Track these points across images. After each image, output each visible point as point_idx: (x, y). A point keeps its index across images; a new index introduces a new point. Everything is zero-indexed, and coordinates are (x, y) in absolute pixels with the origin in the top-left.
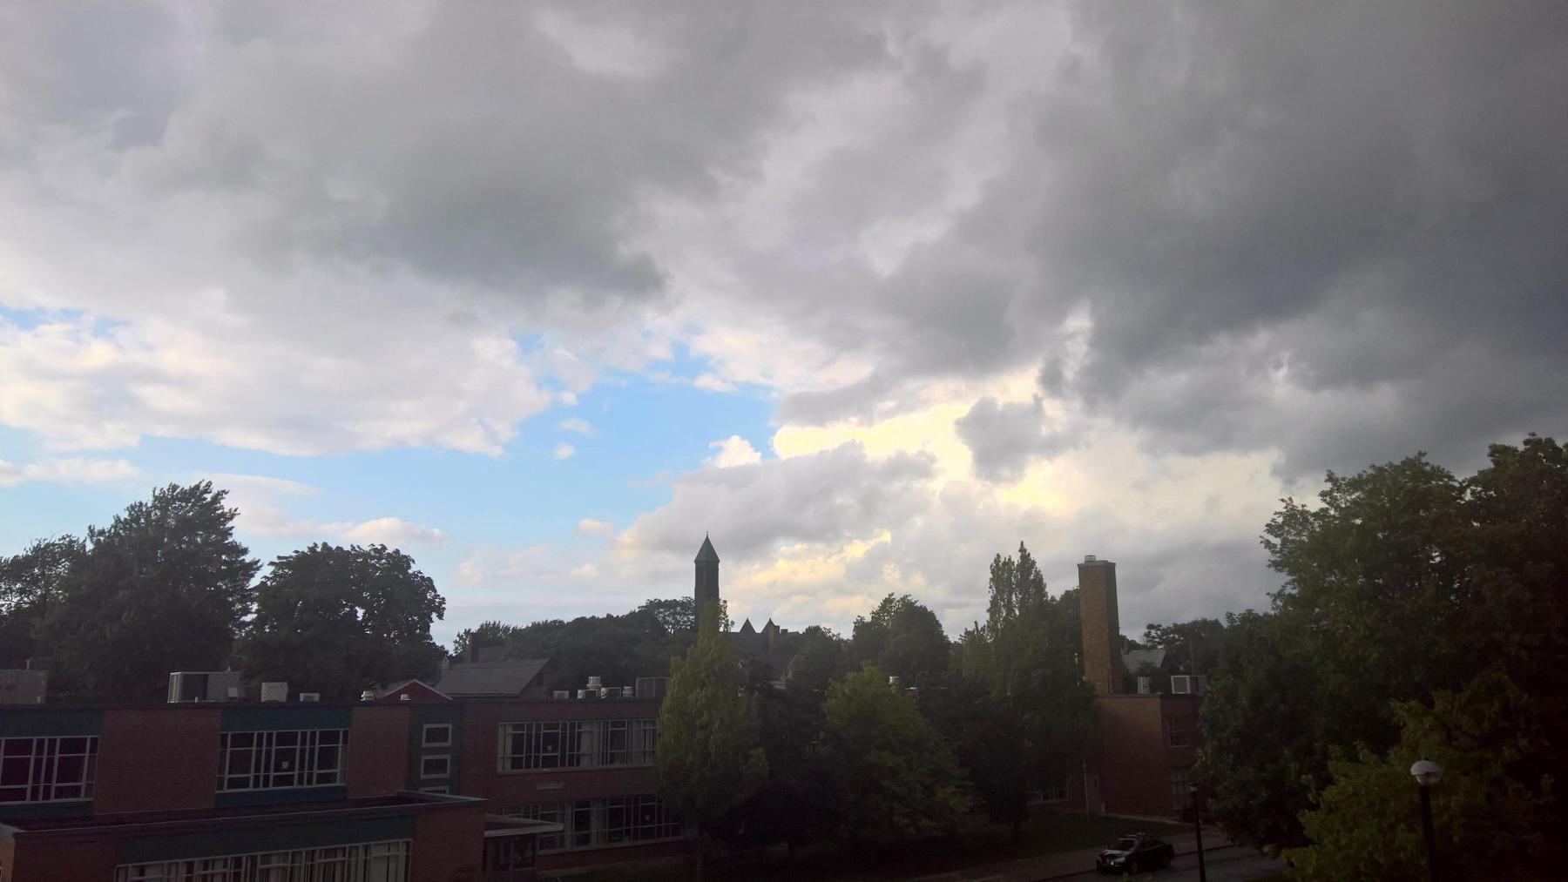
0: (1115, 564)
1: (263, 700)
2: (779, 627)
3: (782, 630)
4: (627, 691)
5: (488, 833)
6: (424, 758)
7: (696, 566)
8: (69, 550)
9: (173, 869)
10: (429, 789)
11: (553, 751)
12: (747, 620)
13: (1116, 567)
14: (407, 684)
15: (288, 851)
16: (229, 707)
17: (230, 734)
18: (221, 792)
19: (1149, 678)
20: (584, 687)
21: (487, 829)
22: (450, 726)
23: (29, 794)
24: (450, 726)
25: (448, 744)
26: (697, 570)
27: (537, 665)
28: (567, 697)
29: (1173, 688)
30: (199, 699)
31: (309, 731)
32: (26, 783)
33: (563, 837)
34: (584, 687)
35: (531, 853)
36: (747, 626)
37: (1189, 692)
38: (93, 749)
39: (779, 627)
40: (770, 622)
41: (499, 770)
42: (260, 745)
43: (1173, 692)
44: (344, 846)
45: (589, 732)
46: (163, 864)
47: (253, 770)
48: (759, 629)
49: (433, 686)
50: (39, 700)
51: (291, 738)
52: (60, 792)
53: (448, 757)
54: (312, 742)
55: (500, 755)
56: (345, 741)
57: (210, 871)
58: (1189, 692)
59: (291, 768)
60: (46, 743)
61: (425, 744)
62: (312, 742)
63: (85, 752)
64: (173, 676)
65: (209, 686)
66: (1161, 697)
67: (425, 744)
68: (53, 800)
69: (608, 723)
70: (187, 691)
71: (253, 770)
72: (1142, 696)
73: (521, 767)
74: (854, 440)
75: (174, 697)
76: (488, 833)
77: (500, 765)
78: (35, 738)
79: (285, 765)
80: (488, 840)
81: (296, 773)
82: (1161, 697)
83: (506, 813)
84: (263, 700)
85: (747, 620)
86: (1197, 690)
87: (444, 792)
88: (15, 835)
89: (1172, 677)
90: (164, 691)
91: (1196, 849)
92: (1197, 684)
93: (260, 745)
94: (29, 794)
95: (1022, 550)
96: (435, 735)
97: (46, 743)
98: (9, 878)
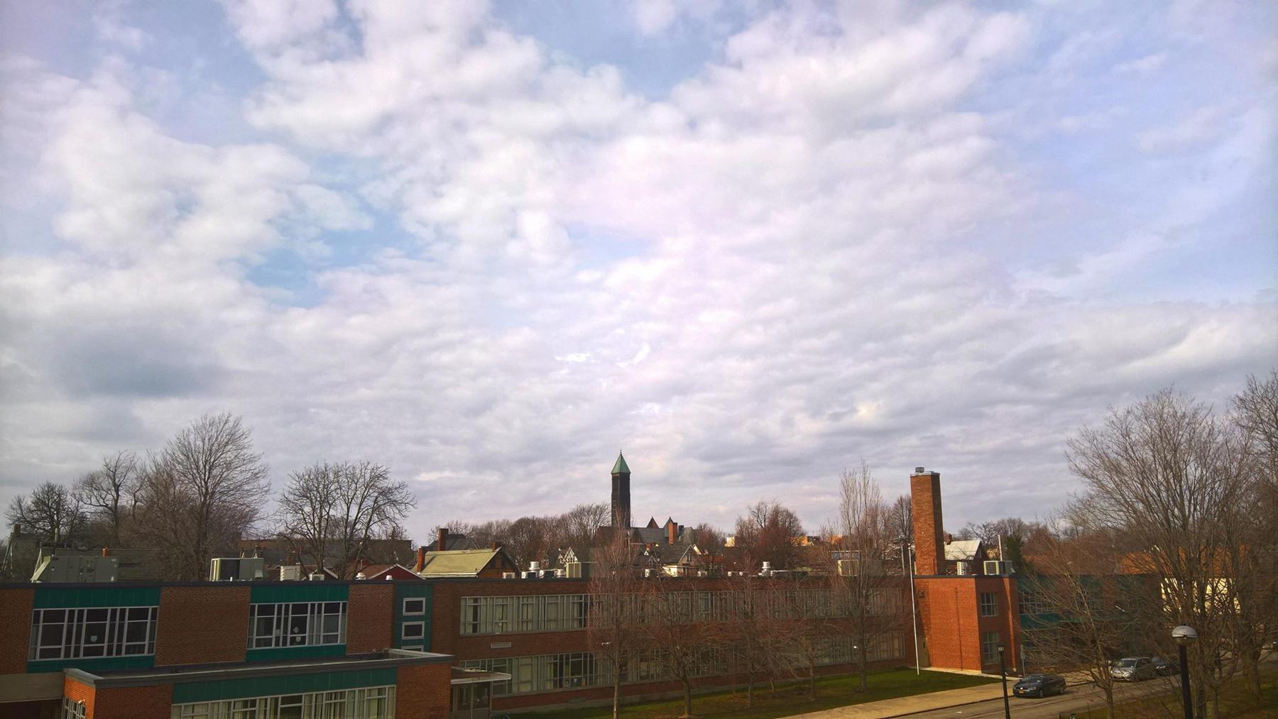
0: (939, 474)
1: (282, 579)
2: (677, 524)
5: (454, 681)
9: (216, 707)
10: (408, 647)
11: (97, 642)
12: (652, 519)
15: (208, 702)
16: (256, 584)
17: (257, 605)
18: (111, 657)
20: (527, 570)
21: (453, 679)
22: (423, 599)
23: (105, 651)
24: (423, 599)
25: (423, 613)
26: (613, 479)
30: (233, 579)
31: (284, 604)
32: (60, 644)
33: (511, 684)
34: (527, 570)
35: (487, 697)
37: (998, 573)
38: (154, 617)
39: (677, 524)
41: (462, 632)
42: (279, 613)
43: (986, 574)
44: (266, 697)
46: (208, 704)
47: (147, 638)
48: (661, 524)
50: (112, 579)
51: (102, 615)
52: (128, 650)
54: (287, 613)
55: (462, 620)
56: (344, 611)
57: (333, 701)
59: (101, 640)
61: (405, 613)
62: (287, 613)
63: (64, 622)
64: (214, 561)
65: (240, 569)
66: (975, 577)
67: (405, 613)
68: (123, 655)
70: (223, 573)
71: (147, 638)
72: (960, 577)
75: (215, 576)
76: (454, 681)
77: (462, 627)
78: (110, 609)
79: (94, 638)
80: (453, 688)
81: (105, 645)
82: (975, 577)
83: (467, 667)
84: (282, 579)
85: (652, 519)
87: (420, 650)
88: (96, 682)
89: (985, 562)
90: (206, 570)
91: (1003, 696)
93: (279, 613)
94: (105, 651)
95: (250, 431)
98: (90, 710)
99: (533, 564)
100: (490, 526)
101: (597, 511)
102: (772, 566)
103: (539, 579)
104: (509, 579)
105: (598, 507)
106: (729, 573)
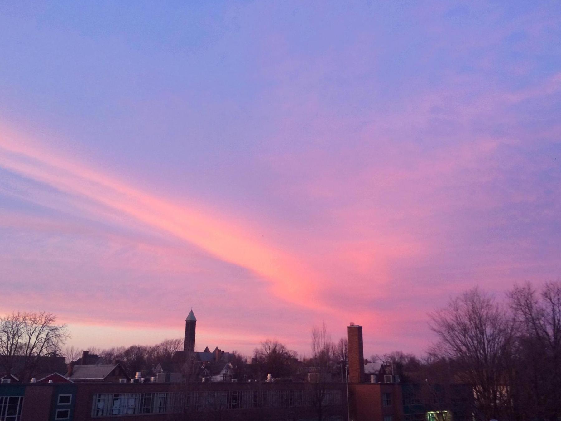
2: (220, 350)
3: (222, 352)
4: (152, 379)
6: (58, 410)
7: (186, 323)
8: (235, 359)
13: (362, 328)
14: (53, 374)
17: (9, 397)
19: (375, 376)
27: (110, 368)
28: (125, 382)
29: (385, 380)
36: (207, 350)
40: (217, 348)
43: (385, 382)
45: (103, 399)
48: (212, 350)
49: (63, 375)
53: (69, 410)
58: (392, 382)
60: (4, 399)
67: (59, 404)
69: (143, 394)
73: (149, 412)
74: (347, 327)
86: (395, 381)
92: (395, 379)
96: (66, 399)
97: (4, 399)
99: (137, 374)
100: (113, 349)
101: (178, 342)
102: (273, 376)
103: (141, 384)
104: (123, 384)
105: (177, 340)
106: (249, 380)
